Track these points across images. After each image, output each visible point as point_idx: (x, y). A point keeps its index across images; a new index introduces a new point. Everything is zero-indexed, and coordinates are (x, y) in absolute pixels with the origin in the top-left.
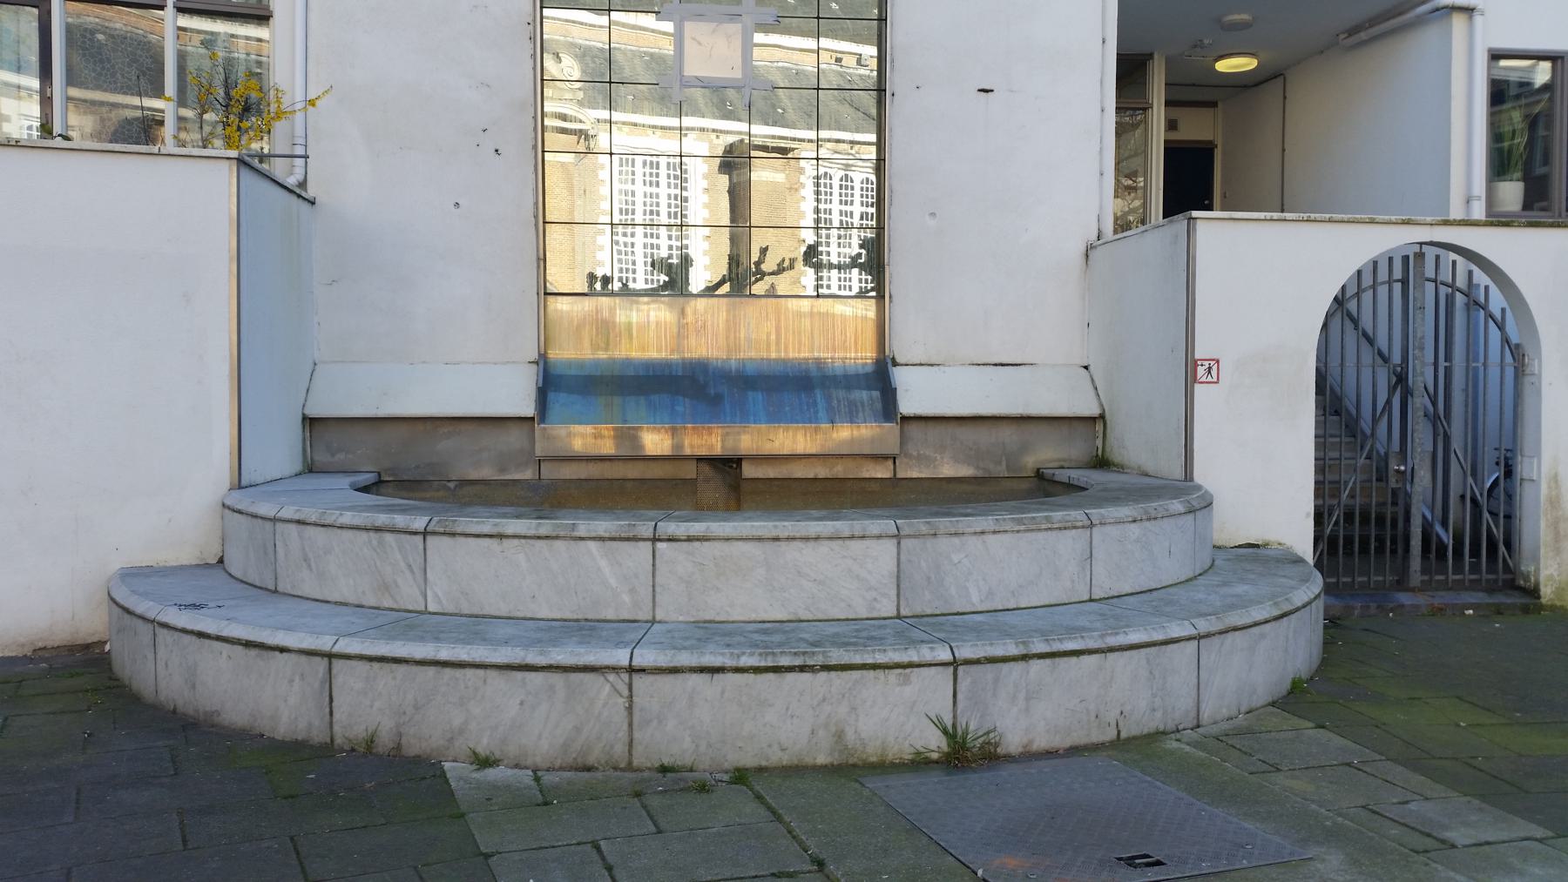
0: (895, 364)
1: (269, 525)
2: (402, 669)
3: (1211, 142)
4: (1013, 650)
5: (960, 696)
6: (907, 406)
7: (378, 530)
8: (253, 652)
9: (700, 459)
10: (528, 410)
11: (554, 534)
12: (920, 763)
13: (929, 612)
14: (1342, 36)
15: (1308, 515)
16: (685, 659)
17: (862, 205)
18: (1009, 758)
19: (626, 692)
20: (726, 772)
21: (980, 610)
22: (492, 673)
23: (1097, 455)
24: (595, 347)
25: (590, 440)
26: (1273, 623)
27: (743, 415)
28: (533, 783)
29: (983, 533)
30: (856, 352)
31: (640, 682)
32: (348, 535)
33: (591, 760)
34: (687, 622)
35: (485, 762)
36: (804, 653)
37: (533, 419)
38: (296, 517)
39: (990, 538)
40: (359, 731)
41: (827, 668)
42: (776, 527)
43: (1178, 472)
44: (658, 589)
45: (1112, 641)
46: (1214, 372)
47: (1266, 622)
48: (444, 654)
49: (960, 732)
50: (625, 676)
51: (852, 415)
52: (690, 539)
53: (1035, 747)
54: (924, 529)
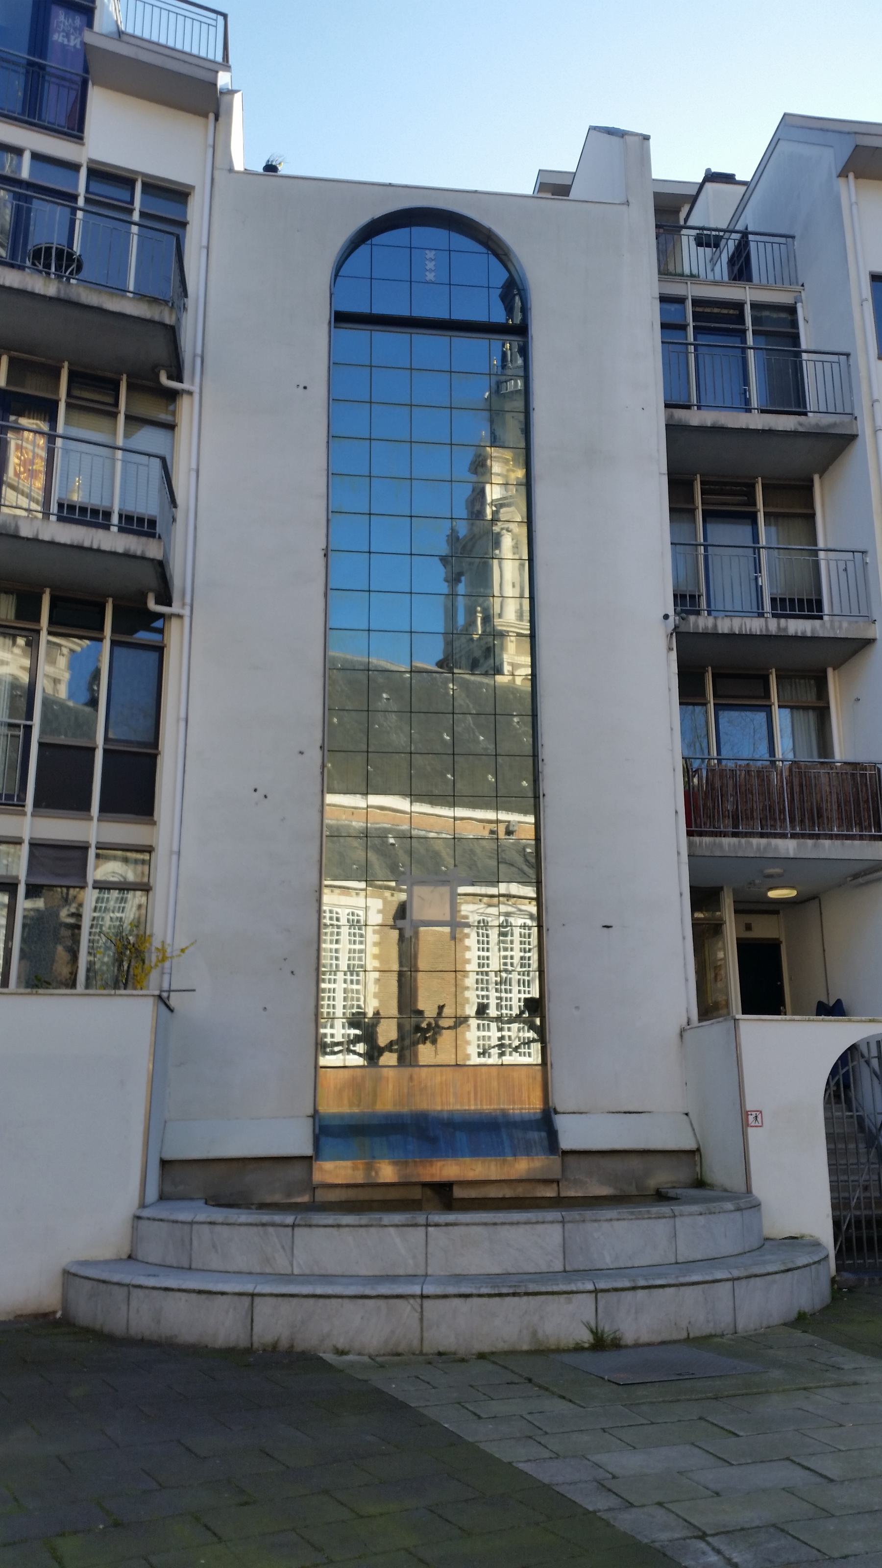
0: (556, 1112)
1: (186, 1228)
2: (295, 1301)
3: (778, 939)
4: (627, 1284)
5: (599, 1311)
6: (566, 1142)
7: (263, 1225)
8: (203, 1297)
9: (425, 1185)
10: (308, 1151)
11: (370, 1224)
12: (578, 1349)
13: (582, 1268)
14: (849, 879)
15: (828, 1216)
16: (451, 1290)
17: (521, 951)
18: (626, 1346)
19: (419, 1310)
20: (473, 1355)
21: (612, 1267)
22: (346, 1301)
23: (698, 1179)
24: (351, 1104)
25: (350, 1172)
26: (782, 1274)
27: (453, 1152)
28: (371, 1361)
29: (611, 1220)
30: (529, 1104)
31: (427, 1303)
32: (243, 1229)
33: (400, 1350)
34: (445, 1276)
35: (341, 1353)
36: (515, 1286)
37: (311, 1157)
38: (209, 1220)
39: (615, 1223)
40: (269, 1338)
41: (527, 1294)
42: (494, 1217)
43: (743, 1189)
44: (429, 1256)
45: (682, 1280)
46: (759, 1119)
47: (776, 1273)
48: (319, 1291)
49: (599, 1331)
50: (419, 1300)
51: (527, 1150)
52: (447, 1225)
53: (641, 1341)
54: (577, 1217)
